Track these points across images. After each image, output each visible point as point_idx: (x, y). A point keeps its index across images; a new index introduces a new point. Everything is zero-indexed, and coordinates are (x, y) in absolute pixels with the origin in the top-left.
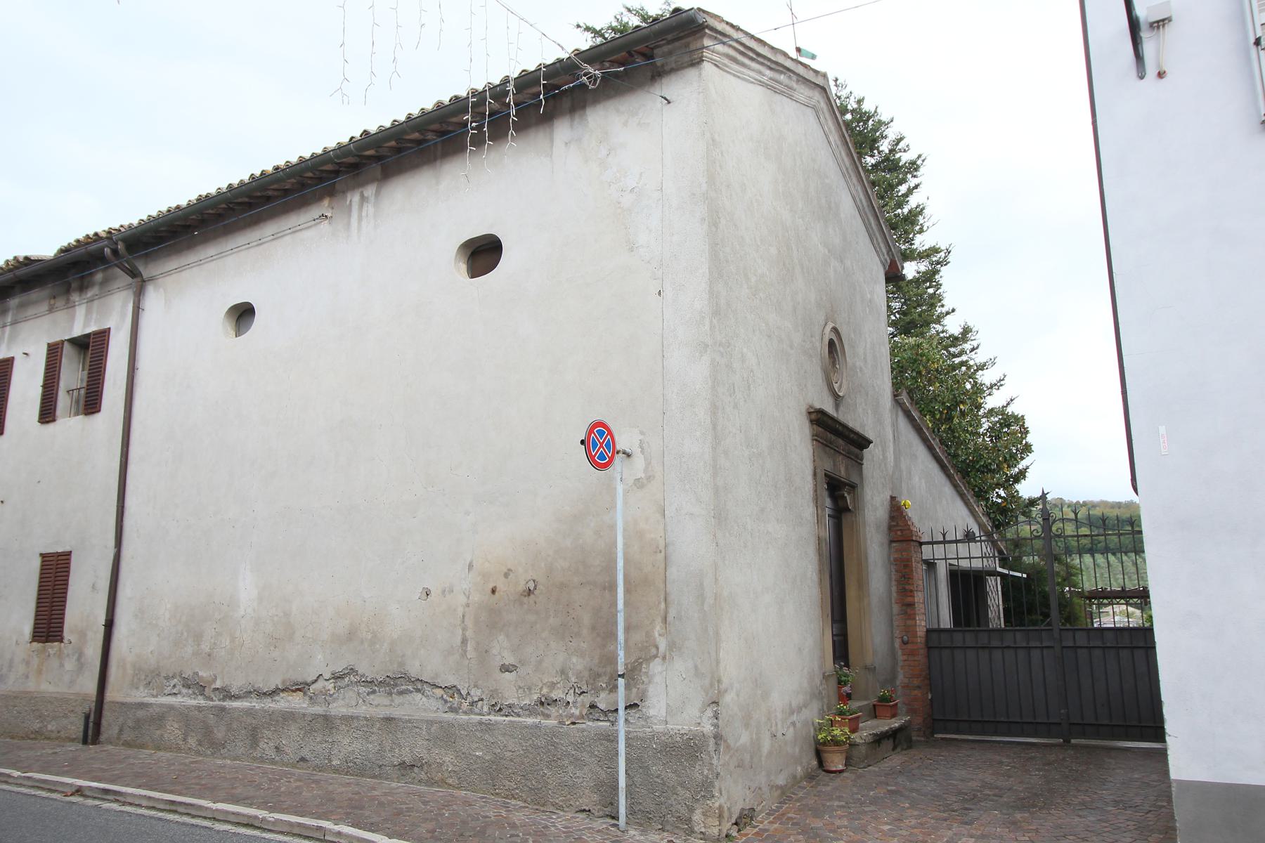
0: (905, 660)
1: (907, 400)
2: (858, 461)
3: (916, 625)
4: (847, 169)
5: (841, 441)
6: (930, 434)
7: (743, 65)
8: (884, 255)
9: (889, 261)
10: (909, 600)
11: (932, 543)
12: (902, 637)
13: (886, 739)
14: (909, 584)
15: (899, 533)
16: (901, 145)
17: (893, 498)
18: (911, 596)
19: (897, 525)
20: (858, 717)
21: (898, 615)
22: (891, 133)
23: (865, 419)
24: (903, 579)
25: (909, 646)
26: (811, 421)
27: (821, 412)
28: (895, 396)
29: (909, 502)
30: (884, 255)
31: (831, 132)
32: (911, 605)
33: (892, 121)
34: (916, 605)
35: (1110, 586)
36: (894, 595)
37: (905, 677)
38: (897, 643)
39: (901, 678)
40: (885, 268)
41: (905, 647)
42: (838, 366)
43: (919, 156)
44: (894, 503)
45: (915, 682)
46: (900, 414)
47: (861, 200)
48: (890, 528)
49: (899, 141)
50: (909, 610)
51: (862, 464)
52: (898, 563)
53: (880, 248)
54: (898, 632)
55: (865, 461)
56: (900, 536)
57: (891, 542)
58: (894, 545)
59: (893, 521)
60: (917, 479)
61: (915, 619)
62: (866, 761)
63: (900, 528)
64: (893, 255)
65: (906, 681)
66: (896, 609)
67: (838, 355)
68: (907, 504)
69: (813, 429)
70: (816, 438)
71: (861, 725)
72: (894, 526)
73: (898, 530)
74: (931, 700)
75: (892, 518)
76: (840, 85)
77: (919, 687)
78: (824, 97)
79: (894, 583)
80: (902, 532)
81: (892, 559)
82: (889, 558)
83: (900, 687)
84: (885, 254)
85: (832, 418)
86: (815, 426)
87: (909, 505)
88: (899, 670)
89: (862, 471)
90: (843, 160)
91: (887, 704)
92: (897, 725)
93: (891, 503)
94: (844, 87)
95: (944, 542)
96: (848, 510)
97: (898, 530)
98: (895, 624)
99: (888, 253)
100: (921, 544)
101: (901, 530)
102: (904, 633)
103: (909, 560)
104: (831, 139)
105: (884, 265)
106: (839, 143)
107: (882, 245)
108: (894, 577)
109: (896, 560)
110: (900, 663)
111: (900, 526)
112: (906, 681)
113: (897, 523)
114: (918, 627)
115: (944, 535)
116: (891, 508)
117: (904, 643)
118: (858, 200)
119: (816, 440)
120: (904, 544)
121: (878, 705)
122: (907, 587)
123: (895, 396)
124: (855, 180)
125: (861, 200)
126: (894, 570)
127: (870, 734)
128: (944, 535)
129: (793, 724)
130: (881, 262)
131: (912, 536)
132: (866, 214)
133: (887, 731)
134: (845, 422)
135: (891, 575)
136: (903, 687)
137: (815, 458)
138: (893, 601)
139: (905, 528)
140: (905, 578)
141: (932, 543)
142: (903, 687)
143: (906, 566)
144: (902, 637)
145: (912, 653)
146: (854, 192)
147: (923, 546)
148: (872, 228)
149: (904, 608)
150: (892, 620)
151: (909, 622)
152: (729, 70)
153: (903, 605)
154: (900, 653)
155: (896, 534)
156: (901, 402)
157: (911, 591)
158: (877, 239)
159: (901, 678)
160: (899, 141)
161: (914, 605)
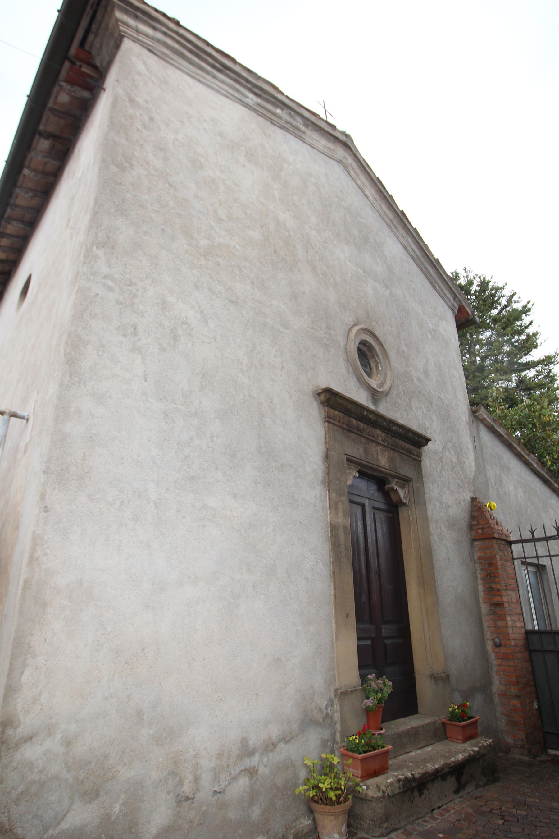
0: (499, 665)
1: (486, 415)
2: (417, 461)
3: (507, 626)
4: (391, 221)
5: (379, 432)
6: (522, 449)
7: (207, 72)
8: (450, 301)
9: (457, 307)
10: (497, 599)
11: (522, 541)
12: (494, 639)
13: (449, 776)
14: (495, 583)
15: (480, 531)
16: (515, 298)
17: (473, 499)
18: (498, 595)
19: (478, 523)
20: (387, 752)
21: (487, 615)
22: (507, 292)
23: (427, 423)
24: (489, 577)
25: (503, 650)
26: (322, 403)
27: (329, 392)
28: (474, 412)
29: (494, 504)
30: (450, 301)
31: (365, 186)
32: (500, 605)
33: (506, 284)
34: (506, 605)
35: (470, 835)
36: (481, 594)
37: (501, 683)
38: (489, 646)
39: (497, 685)
40: (454, 312)
41: (497, 650)
42: (380, 368)
43: (528, 302)
44: (475, 503)
45: (513, 690)
46: (482, 428)
47: (413, 250)
48: (471, 527)
49: (512, 296)
50: (498, 610)
51: (421, 461)
52: (483, 561)
53: (444, 294)
54: (489, 633)
55: (423, 458)
56: (482, 534)
57: (474, 540)
58: (476, 543)
59: (474, 520)
60: (511, 488)
61: (504, 619)
62: (385, 825)
63: (481, 526)
64: (460, 301)
65: (503, 688)
66: (484, 608)
67: (379, 359)
68: (492, 506)
69: (325, 411)
70: (329, 420)
71: (390, 762)
72: (476, 525)
73: (480, 529)
74: (539, 709)
75: (473, 517)
76: (468, 271)
77: (517, 696)
78: (350, 155)
79: (480, 582)
80: (483, 531)
81: (476, 557)
82: (472, 558)
83: (496, 695)
84: (452, 299)
85: (372, 412)
86: (326, 408)
87: (494, 506)
88: (494, 675)
89: (421, 471)
90: (385, 213)
91: (458, 723)
92: (460, 757)
93: (472, 503)
94: (471, 271)
95: (533, 540)
96: (401, 503)
97: (480, 529)
98: (485, 624)
99: (454, 299)
100: (510, 543)
101: (481, 528)
102: (496, 635)
103: (493, 558)
104: (367, 192)
105: (452, 310)
106: (378, 197)
107: (446, 292)
108: (479, 576)
109: (479, 558)
110: (495, 669)
111: (482, 524)
112: (503, 688)
113: (478, 522)
114: (509, 629)
115: (533, 533)
116: (472, 508)
117: (498, 646)
118: (410, 249)
119: (328, 422)
120: (487, 543)
121: (447, 724)
122: (494, 586)
123: (474, 413)
124: (402, 231)
125: (413, 250)
126: (479, 569)
127: (399, 780)
128: (533, 533)
129: (252, 772)
130: (449, 306)
131: (493, 533)
132: (422, 263)
133: (441, 769)
134: (395, 420)
135: (476, 573)
136: (500, 695)
137: (327, 440)
138: (481, 600)
139: (486, 525)
140: (490, 576)
141: (522, 541)
142: (500, 695)
143: (490, 564)
144: (494, 639)
145: (505, 657)
146: (406, 244)
147: (513, 546)
148: (432, 276)
149: (493, 608)
150: (481, 621)
151: (499, 623)
152: (180, 67)
153: (491, 605)
154: (493, 656)
155: (477, 532)
156: (481, 418)
157: (498, 590)
158: (439, 286)
159: (497, 685)
160: (512, 296)
161: (503, 604)
